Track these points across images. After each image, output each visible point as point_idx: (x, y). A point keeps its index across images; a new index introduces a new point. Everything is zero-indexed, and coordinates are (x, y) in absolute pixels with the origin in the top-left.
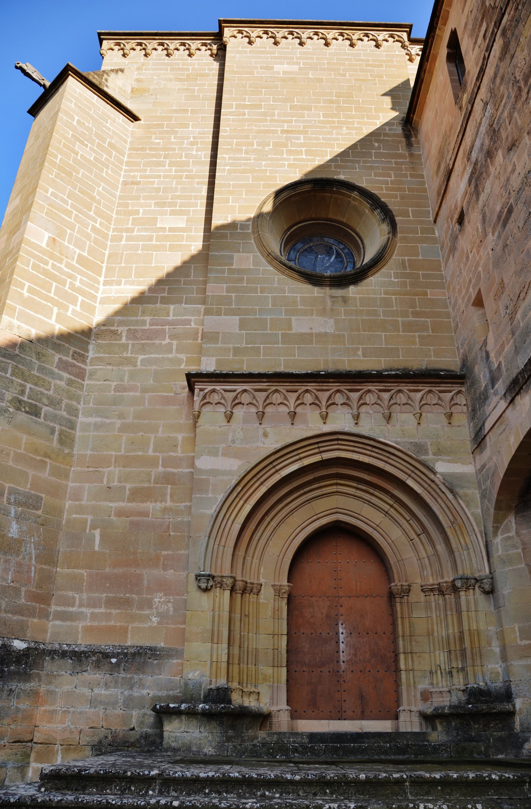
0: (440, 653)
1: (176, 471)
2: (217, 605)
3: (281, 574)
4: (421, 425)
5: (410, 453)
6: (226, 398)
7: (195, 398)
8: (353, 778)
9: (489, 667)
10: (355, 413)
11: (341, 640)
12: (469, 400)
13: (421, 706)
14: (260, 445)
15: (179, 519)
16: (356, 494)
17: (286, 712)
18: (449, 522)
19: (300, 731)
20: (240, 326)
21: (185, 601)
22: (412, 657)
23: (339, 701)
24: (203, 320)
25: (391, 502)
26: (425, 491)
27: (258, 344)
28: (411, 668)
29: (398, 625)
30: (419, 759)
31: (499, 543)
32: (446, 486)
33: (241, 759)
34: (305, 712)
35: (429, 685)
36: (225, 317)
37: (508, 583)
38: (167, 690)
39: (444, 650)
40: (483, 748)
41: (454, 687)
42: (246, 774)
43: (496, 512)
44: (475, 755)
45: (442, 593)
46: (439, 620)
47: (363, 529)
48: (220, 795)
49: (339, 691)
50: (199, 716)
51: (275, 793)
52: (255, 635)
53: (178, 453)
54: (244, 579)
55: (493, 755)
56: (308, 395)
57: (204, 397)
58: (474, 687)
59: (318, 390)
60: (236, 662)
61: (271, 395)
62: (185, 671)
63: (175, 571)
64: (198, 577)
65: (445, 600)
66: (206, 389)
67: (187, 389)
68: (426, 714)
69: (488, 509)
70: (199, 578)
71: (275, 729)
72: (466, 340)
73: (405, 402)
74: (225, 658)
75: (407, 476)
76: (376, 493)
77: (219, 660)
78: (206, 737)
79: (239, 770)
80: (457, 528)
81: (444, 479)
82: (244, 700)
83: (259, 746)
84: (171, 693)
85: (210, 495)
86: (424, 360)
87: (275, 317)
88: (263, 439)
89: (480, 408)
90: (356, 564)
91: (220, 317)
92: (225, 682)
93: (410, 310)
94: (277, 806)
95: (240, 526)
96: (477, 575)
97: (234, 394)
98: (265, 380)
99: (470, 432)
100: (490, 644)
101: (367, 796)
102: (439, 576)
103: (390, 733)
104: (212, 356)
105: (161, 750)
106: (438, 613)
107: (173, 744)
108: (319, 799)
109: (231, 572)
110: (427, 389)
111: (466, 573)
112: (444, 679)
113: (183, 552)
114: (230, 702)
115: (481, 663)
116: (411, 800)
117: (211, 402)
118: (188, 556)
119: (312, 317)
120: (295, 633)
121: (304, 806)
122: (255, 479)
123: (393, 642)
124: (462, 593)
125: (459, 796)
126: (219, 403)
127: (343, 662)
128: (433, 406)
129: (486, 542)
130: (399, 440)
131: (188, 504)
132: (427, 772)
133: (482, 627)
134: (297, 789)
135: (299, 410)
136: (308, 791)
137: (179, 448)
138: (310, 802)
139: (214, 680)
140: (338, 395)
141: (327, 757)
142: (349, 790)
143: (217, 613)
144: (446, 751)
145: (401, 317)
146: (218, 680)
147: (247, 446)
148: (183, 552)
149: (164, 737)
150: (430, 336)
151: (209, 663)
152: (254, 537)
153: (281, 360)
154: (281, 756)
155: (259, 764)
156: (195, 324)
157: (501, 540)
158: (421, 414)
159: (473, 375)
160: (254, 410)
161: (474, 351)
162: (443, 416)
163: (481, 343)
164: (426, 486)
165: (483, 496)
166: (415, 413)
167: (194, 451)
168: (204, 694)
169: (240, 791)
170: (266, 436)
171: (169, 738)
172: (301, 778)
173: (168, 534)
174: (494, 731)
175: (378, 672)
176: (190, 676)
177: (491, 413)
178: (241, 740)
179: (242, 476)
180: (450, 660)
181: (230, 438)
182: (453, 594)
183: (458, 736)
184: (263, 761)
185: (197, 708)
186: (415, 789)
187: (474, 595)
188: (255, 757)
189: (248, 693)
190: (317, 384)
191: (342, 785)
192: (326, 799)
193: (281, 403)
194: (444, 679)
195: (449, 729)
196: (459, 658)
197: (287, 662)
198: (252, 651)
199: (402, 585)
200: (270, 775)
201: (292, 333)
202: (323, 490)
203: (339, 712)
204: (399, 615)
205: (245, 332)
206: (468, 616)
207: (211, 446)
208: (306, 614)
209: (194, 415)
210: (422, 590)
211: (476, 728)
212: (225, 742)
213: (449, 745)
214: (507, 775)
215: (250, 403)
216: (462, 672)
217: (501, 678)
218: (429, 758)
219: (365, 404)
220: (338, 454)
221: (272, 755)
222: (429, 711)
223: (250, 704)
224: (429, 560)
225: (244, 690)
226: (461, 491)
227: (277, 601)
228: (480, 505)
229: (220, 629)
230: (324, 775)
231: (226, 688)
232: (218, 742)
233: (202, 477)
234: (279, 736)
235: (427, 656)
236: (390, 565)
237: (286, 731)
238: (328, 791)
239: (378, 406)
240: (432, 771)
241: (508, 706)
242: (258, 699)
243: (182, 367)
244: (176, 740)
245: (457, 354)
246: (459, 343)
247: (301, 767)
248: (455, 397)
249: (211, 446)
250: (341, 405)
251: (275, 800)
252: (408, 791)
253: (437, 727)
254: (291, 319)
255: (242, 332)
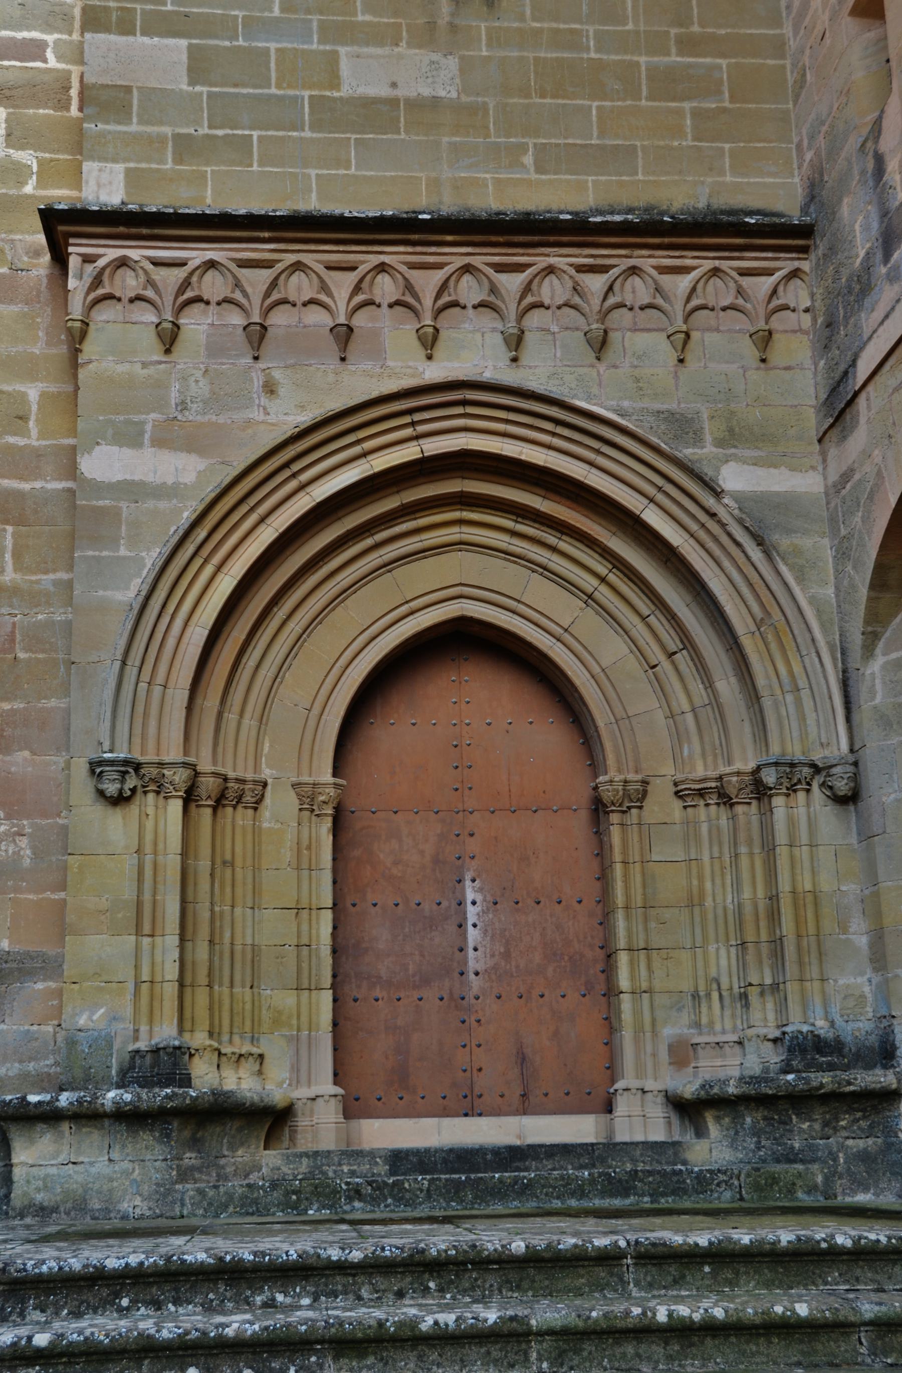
0: (718, 949)
1: (26, 486)
2: (149, 837)
3: (315, 757)
4: (687, 364)
5: (655, 440)
6: (159, 284)
7: (72, 283)
8: (495, 1250)
9: (841, 982)
10: (511, 331)
11: (471, 918)
12: (818, 297)
13: (668, 1078)
14: (256, 415)
15: (40, 617)
16: (512, 549)
17: (333, 1100)
18: (750, 620)
19: (366, 1146)
20: (190, 70)
21: (64, 830)
22: (649, 959)
23: (465, 1071)
24: (82, 43)
25: (602, 570)
26: (692, 541)
27: (243, 128)
28: (644, 985)
29: (613, 880)
30: (661, 1206)
31: (878, 675)
32: (747, 528)
33: (218, 1221)
34: (379, 1099)
35: (690, 1027)
36: (146, 40)
37: (895, 777)
38: (21, 1062)
39: (728, 940)
40: (819, 1179)
41: (750, 1032)
42: (227, 1253)
43: (873, 594)
44: (800, 1195)
45: (726, 800)
46: (717, 868)
47: (529, 638)
48: (159, 1309)
49: (464, 1046)
50: (107, 1122)
51: (299, 1296)
52: (249, 911)
53: (29, 437)
54: (220, 769)
55: (844, 1194)
56: (384, 280)
57: (97, 281)
58: (801, 1032)
59: (413, 266)
60: (203, 979)
61: (283, 276)
62: (68, 1010)
63: (34, 753)
64: (96, 768)
65: (734, 817)
66: (100, 256)
67: (47, 257)
68: (681, 1098)
69: (853, 586)
70: (98, 770)
71: (304, 1143)
72: (823, 123)
73: (646, 301)
74: (171, 972)
75: (646, 502)
76: (563, 546)
77: (158, 978)
78: (127, 1173)
79: (208, 1245)
80: (770, 637)
81: (740, 509)
82: (224, 1075)
83: (262, 1187)
84: (31, 1066)
85: (123, 552)
86: (703, 183)
87: (290, 46)
88: (264, 401)
89: (846, 318)
90: (510, 727)
91: (131, 39)
92: (174, 1031)
93: (673, 31)
94: (304, 1328)
95: (206, 632)
96: (818, 756)
97: (180, 274)
98: (266, 235)
99: (816, 384)
100: (844, 929)
101: (530, 1293)
102: (720, 757)
103: (592, 1145)
104: (115, 160)
105: (7, 1213)
106: (716, 849)
107: (39, 1197)
108: (411, 1306)
109: (186, 753)
110: (708, 265)
111: (789, 749)
112: (727, 1013)
113: (53, 703)
114: (186, 1081)
115: (822, 974)
116: (636, 1298)
117: (117, 295)
118: (68, 712)
119: (396, 50)
120: (354, 905)
121: (373, 1323)
122: (244, 508)
123: (601, 924)
124: (778, 802)
125: (755, 1288)
126: (139, 298)
127: (477, 974)
128: (722, 314)
129: (844, 671)
130: (626, 404)
131: (63, 575)
132: (677, 1231)
133: (826, 884)
134: (354, 1284)
135: (360, 320)
136: (382, 1287)
137: (31, 424)
138: (388, 1313)
139: (144, 1028)
140: (467, 278)
141: (434, 1207)
142: (485, 1281)
143: (149, 859)
144: (730, 1186)
145: (649, 53)
146: (156, 1029)
147: (221, 420)
148: (53, 703)
149: (15, 1179)
150: (724, 110)
151: (130, 986)
152: (244, 661)
153: (309, 176)
154: (318, 1210)
155: (264, 1229)
156: (59, 58)
157: (884, 667)
158: (688, 335)
159: (835, 225)
160: (236, 319)
161: (843, 155)
162: (748, 341)
163: (865, 131)
164: (694, 527)
165: (843, 554)
166: (671, 330)
167: (73, 432)
168: (121, 1065)
169: (211, 1296)
170: (272, 392)
171: (28, 1182)
172: (366, 1256)
173: (10, 656)
174: (848, 1138)
175: (563, 996)
176: (82, 1021)
177: (875, 331)
178: (218, 1175)
179: (208, 500)
180: (743, 966)
181: (174, 396)
182: (754, 803)
183: (759, 1149)
184: (273, 1223)
185: (100, 1101)
186: (646, 1274)
187: (808, 805)
188: (252, 1214)
189: (234, 1058)
190: (409, 249)
191: (467, 1270)
192: (427, 1305)
193: (312, 302)
194: (727, 1013)
195: (737, 1133)
196: (766, 962)
197: (334, 976)
198: (243, 952)
199: (626, 782)
200: (287, 1253)
201: (341, 98)
202: (424, 536)
203: (466, 1097)
204: (617, 857)
205: (205, 89)
206: (792, 858)
207: (122, 418)
208: (382, 856)
209: (69, 330)
210: (676, 793)
211: (804, 1131)
212: (176, 1182)
213: (736, 1172)
214: (873, 1236)
215: (227, 300)
216: (773, 993)
217: (869, 1009)
218: (687, 1204)
219: (539, 305)
220: (464, 440)
221: (296, 1208)
222: (689, 1089)
223: (239, 1084)
224: (696, 717)
225: (223, 1051)
226: (784, 542)
227: (305, 824)
228: (832, 578)
229: (158, 898)
230: (422, 1245)
231: (176, 1048)
232: (157, 1184)
233: (101, 503)
234: (316, 1159)
235: (685, 956)
236: (597, 731)
237: (332, 1147)
238: (432, 1285)
239: (572, 311)
240: (691, 1230)
241: (885, 1076)
242: (260, 1073)
243: (29, 189)
244: (46, 1187)
245: (795, 166)
246: (804, 131)
247: (367, 1231)
248: (781, 288)
249: (122, 418)
250: (475, 307)
251: (298, 1313)
252: (630, 1277)
253: (707, 1128)
254: (336, 53)
255: (198, 88)
